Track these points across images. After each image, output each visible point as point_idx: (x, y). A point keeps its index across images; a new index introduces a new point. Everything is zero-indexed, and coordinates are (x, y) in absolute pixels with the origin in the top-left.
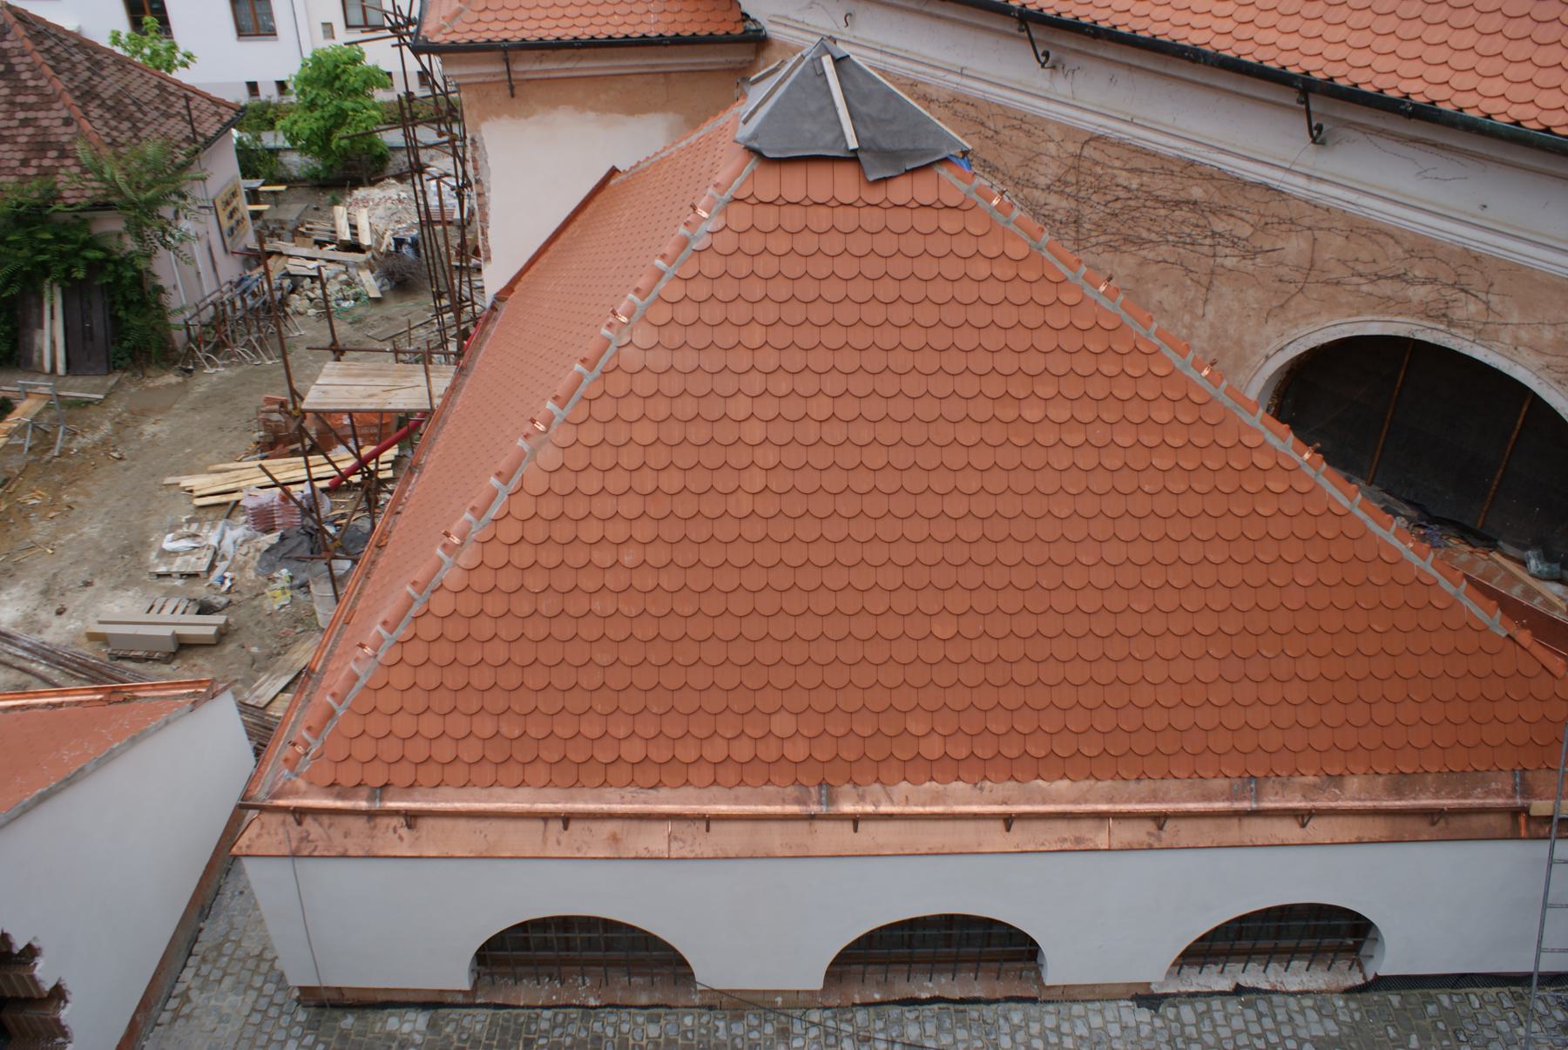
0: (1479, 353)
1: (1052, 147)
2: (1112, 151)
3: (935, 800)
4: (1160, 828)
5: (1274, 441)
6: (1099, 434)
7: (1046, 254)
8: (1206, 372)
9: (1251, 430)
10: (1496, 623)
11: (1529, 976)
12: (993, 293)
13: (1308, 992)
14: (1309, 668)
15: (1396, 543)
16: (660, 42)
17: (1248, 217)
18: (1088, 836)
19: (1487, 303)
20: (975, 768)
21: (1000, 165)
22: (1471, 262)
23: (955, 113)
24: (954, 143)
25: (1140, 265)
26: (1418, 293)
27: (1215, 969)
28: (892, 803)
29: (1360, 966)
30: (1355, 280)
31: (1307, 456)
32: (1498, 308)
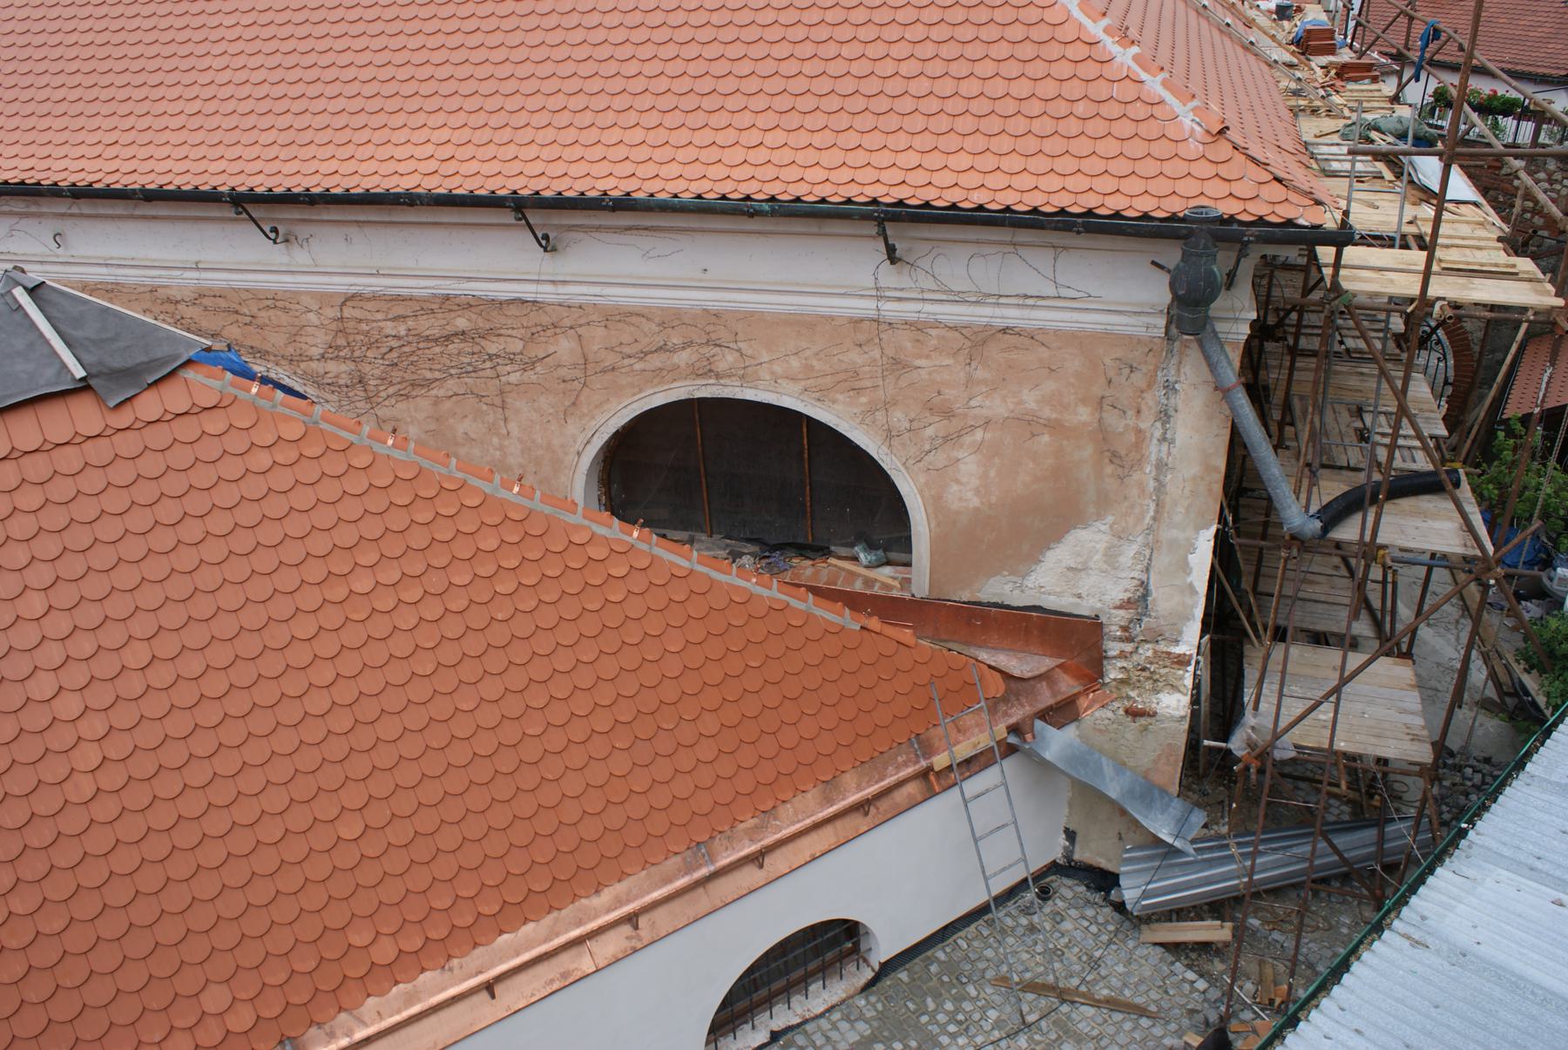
0: (750, 395)
1: (311, 316)
2: (370, 305)
3: (410, 1000)
4: (636, 928)
5: (601, 530)
6: (435, 582)
7: (324, 426)
8: (516, 489)
9: (577, 527)
10: (847, 620)
11: (1026, 880)
12: (282, 480)
13: (833, 1007)
14: (710, 724)
15: (742, 583)
17: (514, 333)
18: (572, 967)
19: (739, 350)
20: (438, 950)
21: (268, 347)
22: (713, 319)
23: (206, 309)
24: (190, 344)
25: (435, 404)
26: (683, 358)
27: (747, 1027)
28: (366, 1025)
29: (865, 961)
30: (627, 362)
31: (636, 534)
32: (749, 352)
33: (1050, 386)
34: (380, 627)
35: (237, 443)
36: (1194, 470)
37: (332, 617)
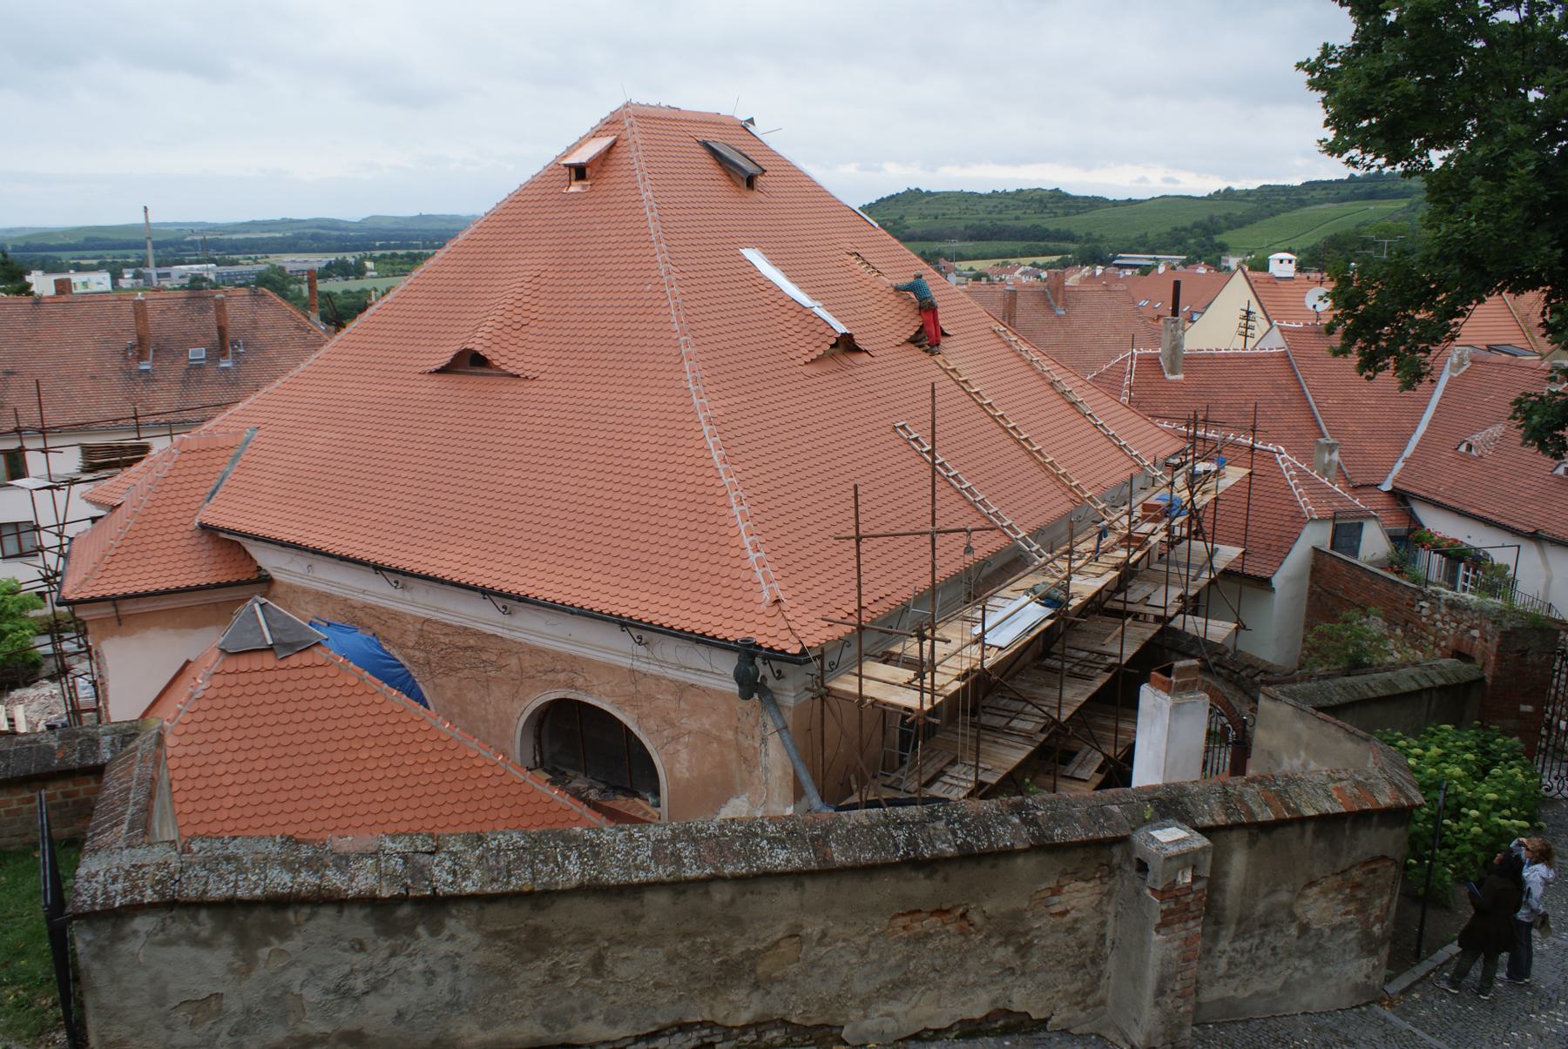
0: (589, 700)
6: (397, 761)
16: (208, 587)
26: (562, 677)
33: (714, 717)
34: (366, 776)
35: (327, 683)
36: (779, 773)
37: (346, 767)
